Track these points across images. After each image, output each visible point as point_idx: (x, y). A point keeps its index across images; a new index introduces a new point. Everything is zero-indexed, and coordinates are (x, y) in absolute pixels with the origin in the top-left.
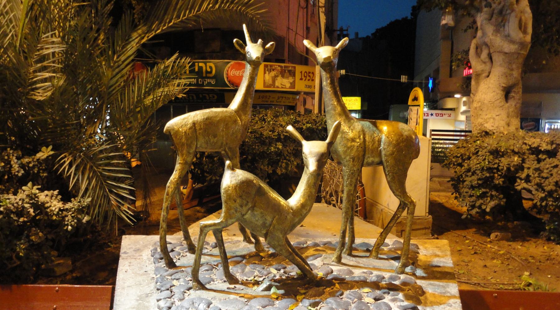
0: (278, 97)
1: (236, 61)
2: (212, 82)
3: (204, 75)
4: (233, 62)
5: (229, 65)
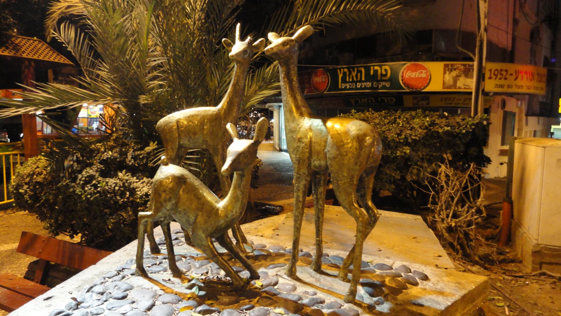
0: (465, 99)
1: (412, 63)
2: (387, 85)
3: (379, 78)
4: (408, 64)
5: (405, 67)
